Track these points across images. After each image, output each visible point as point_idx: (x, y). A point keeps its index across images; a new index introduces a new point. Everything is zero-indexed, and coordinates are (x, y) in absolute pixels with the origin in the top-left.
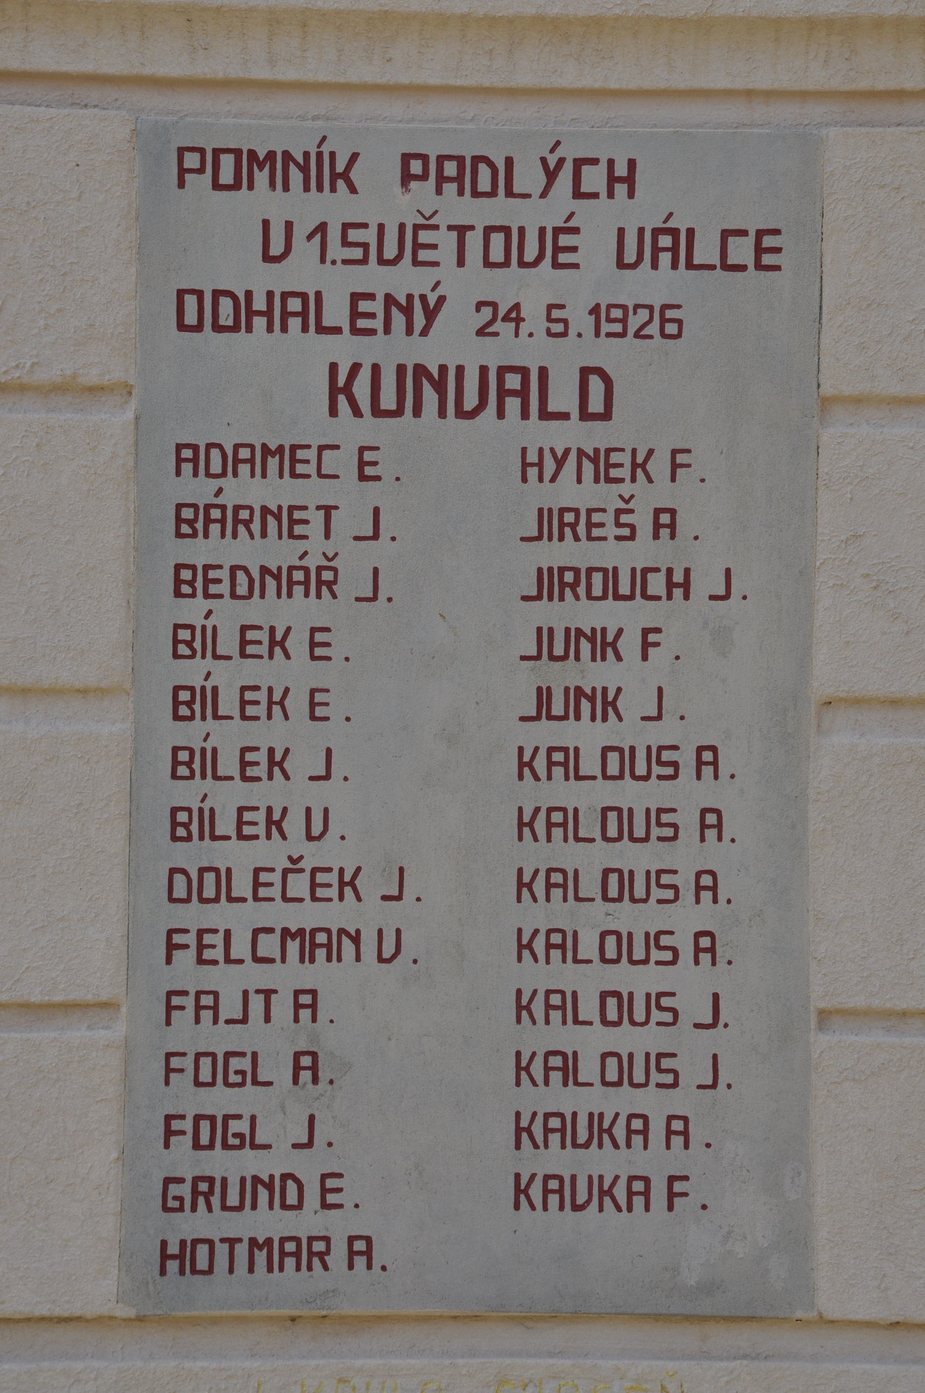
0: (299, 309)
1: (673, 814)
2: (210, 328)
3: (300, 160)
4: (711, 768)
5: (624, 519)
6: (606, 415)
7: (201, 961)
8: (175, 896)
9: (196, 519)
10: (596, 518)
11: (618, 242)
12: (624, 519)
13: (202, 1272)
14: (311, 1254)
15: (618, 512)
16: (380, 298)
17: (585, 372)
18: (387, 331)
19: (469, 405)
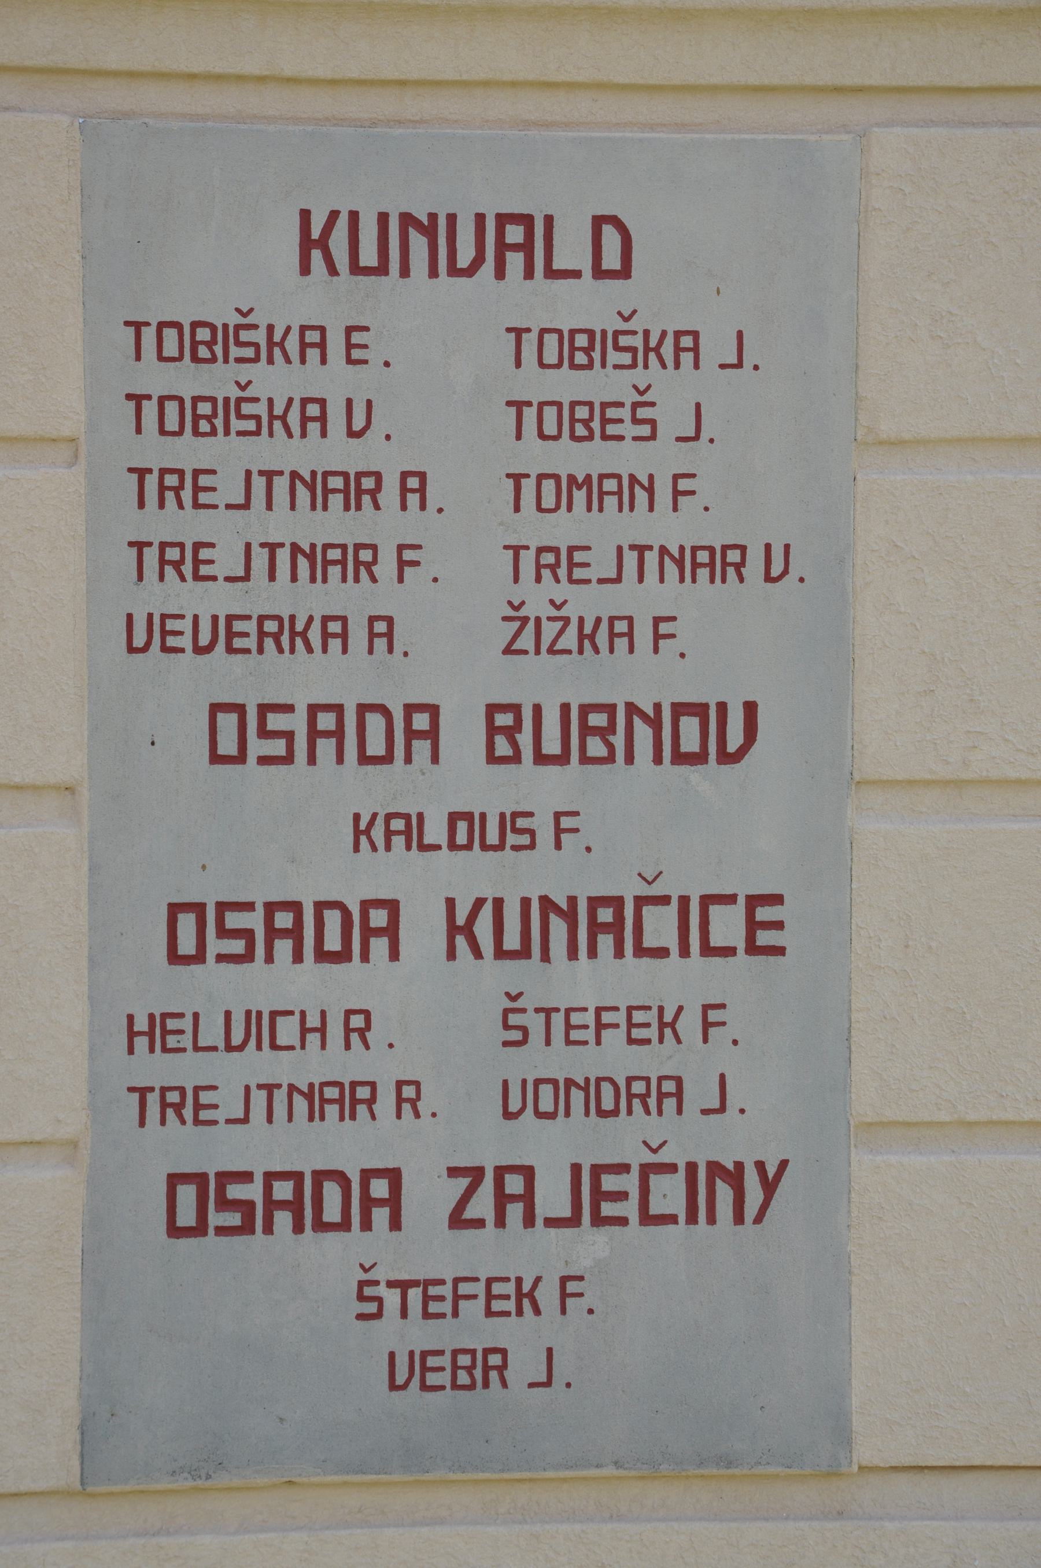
1: (651, 409)
2: (359, 959)
3: (308, 478)
4: (691, 354)
5: (642, 413)
6: (625, 272)
7: (489, 1313)
8: (165, 354)
10: (611, 413)
11: (743, 1202)
12: (642, 413)
14: (357, 563)
15: (635, 406)
17: (598, 222)
19: (463, 262)
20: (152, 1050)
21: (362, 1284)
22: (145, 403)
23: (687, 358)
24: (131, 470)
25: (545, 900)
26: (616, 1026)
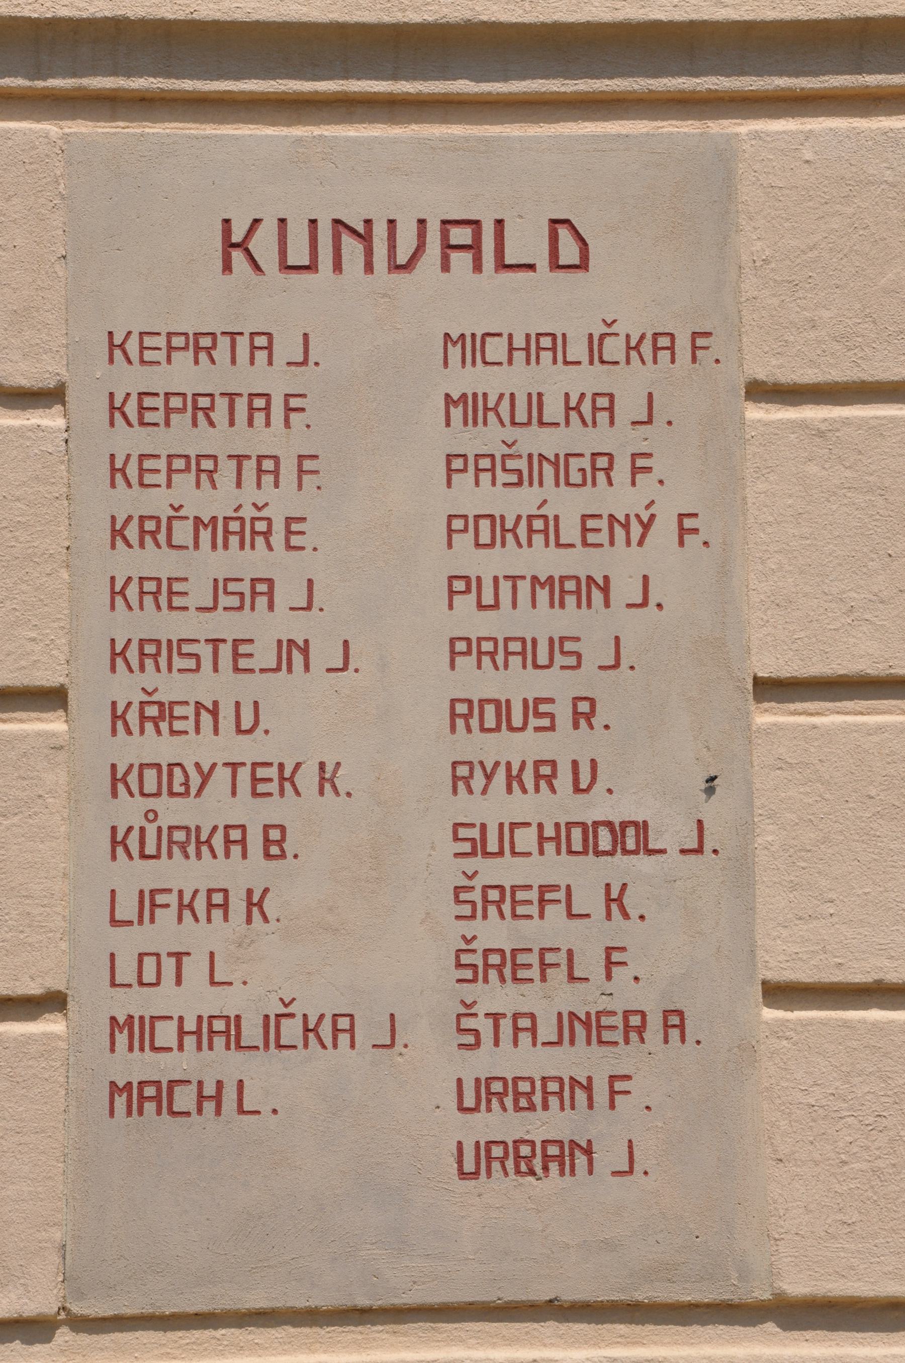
0: (542, 528)
9: (533, 1092)
13: (490, 730)
16: (605, 517)
18: (612, 543)
20: (547, 545)
21: (458, 890)
22: (238, 338)
23: (344, 1039)
24: (681, 543)
25: (572, 1014)
26: (557, 965)
